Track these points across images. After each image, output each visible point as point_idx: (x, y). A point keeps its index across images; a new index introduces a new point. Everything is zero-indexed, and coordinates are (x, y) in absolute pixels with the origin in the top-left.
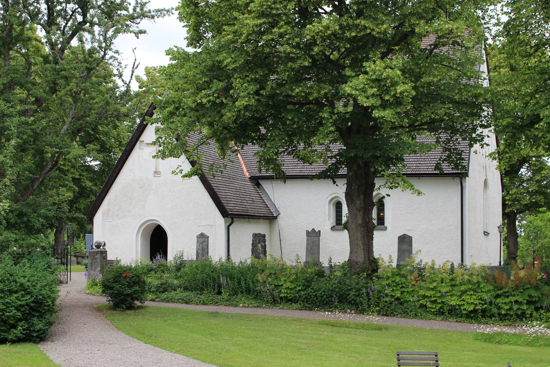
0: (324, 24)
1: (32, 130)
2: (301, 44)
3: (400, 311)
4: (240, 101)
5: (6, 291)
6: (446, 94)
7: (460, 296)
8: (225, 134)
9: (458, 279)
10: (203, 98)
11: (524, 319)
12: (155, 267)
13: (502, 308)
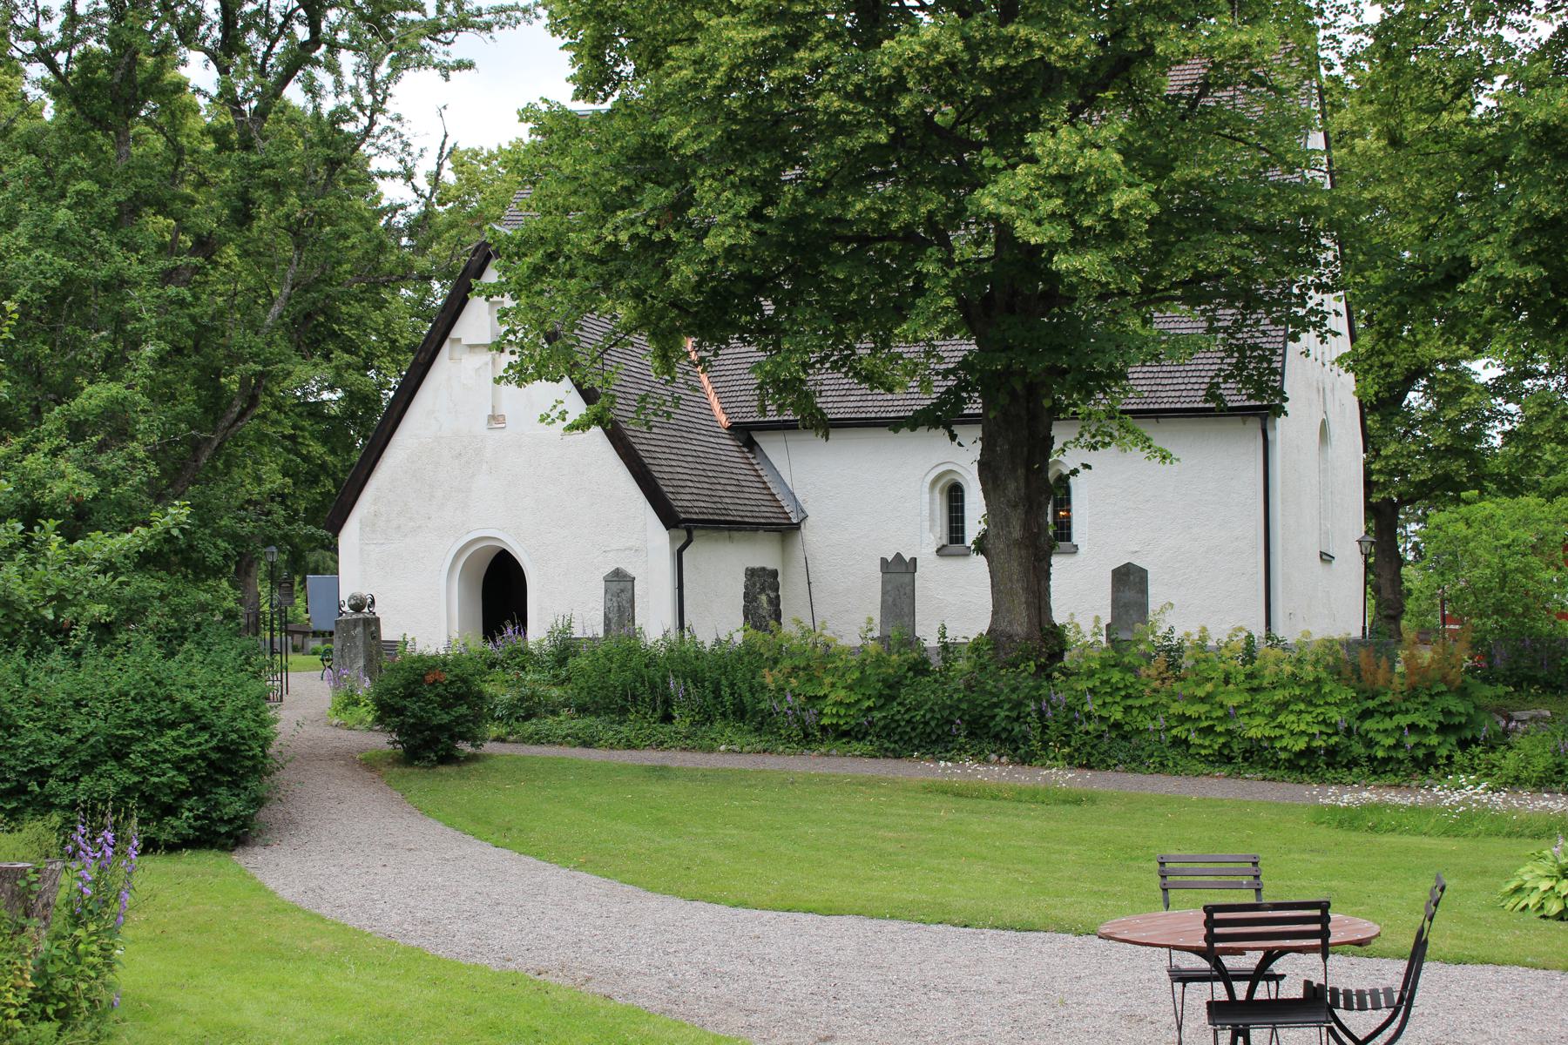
0: (924, 39)
1: (193, 319)
2: (865, 89)
3: (1121, 756)
4: (716, 236)
5: (148, 723)
6: (1234, 208)
7: (1273, 716)
8: (672, 320)
9: (1267, 672)
10: (621, 229)
11: (1432, 770)
12: (501, 656)
13: (1377, 743)
